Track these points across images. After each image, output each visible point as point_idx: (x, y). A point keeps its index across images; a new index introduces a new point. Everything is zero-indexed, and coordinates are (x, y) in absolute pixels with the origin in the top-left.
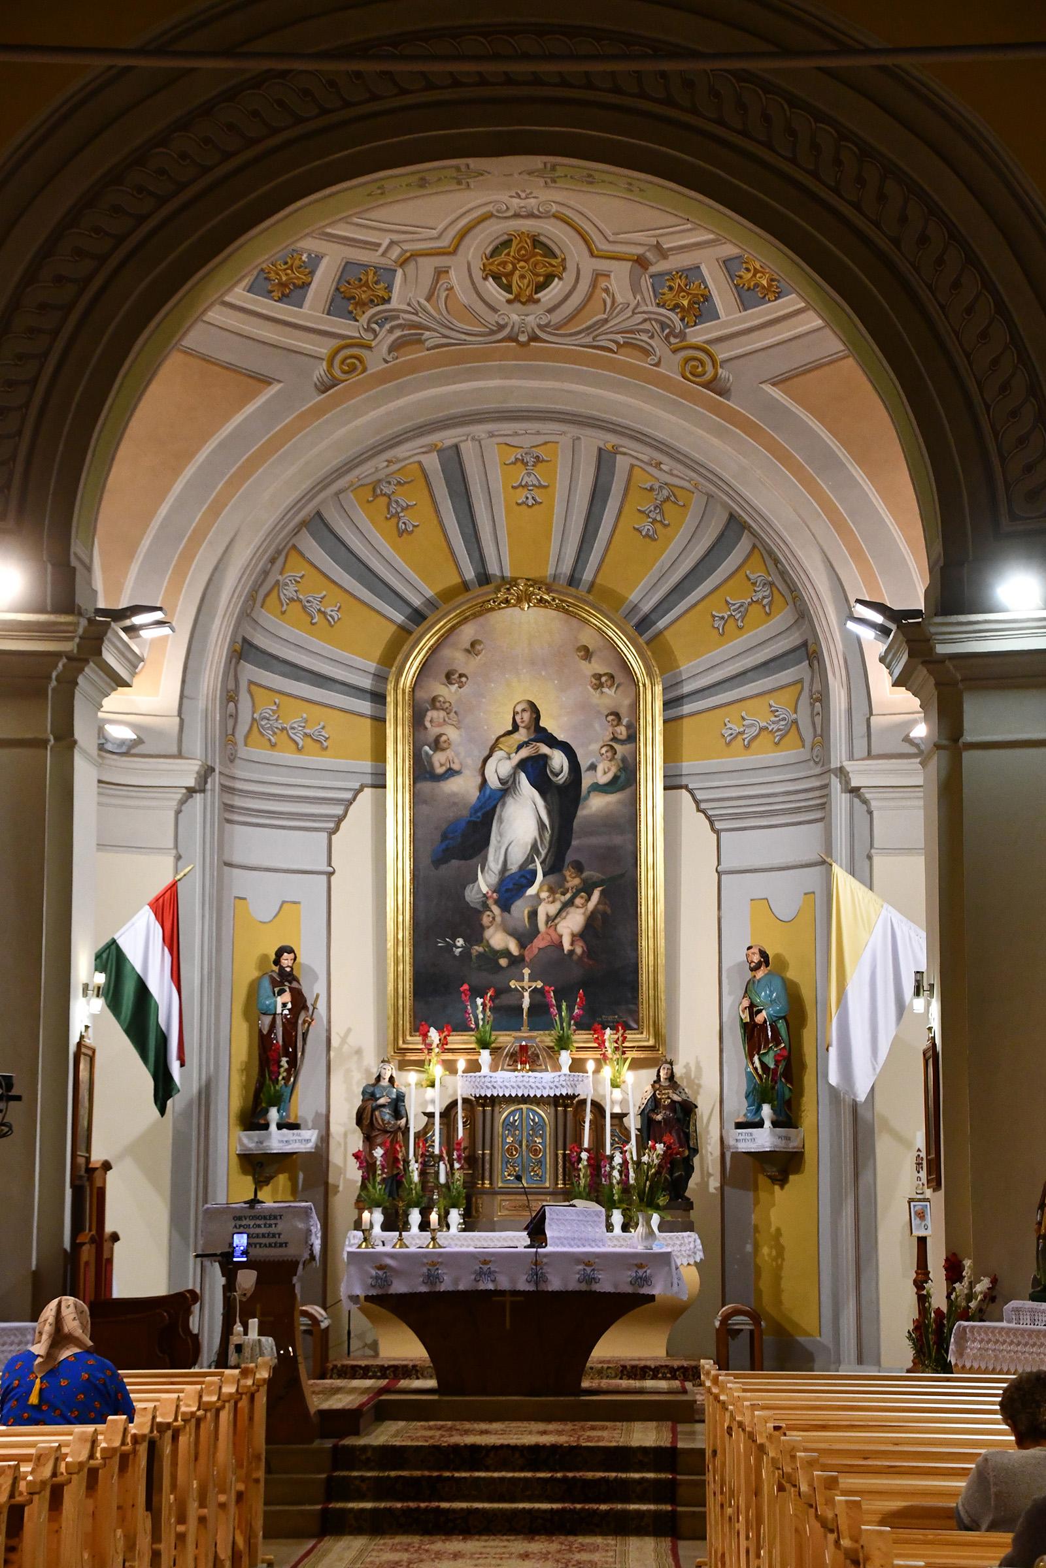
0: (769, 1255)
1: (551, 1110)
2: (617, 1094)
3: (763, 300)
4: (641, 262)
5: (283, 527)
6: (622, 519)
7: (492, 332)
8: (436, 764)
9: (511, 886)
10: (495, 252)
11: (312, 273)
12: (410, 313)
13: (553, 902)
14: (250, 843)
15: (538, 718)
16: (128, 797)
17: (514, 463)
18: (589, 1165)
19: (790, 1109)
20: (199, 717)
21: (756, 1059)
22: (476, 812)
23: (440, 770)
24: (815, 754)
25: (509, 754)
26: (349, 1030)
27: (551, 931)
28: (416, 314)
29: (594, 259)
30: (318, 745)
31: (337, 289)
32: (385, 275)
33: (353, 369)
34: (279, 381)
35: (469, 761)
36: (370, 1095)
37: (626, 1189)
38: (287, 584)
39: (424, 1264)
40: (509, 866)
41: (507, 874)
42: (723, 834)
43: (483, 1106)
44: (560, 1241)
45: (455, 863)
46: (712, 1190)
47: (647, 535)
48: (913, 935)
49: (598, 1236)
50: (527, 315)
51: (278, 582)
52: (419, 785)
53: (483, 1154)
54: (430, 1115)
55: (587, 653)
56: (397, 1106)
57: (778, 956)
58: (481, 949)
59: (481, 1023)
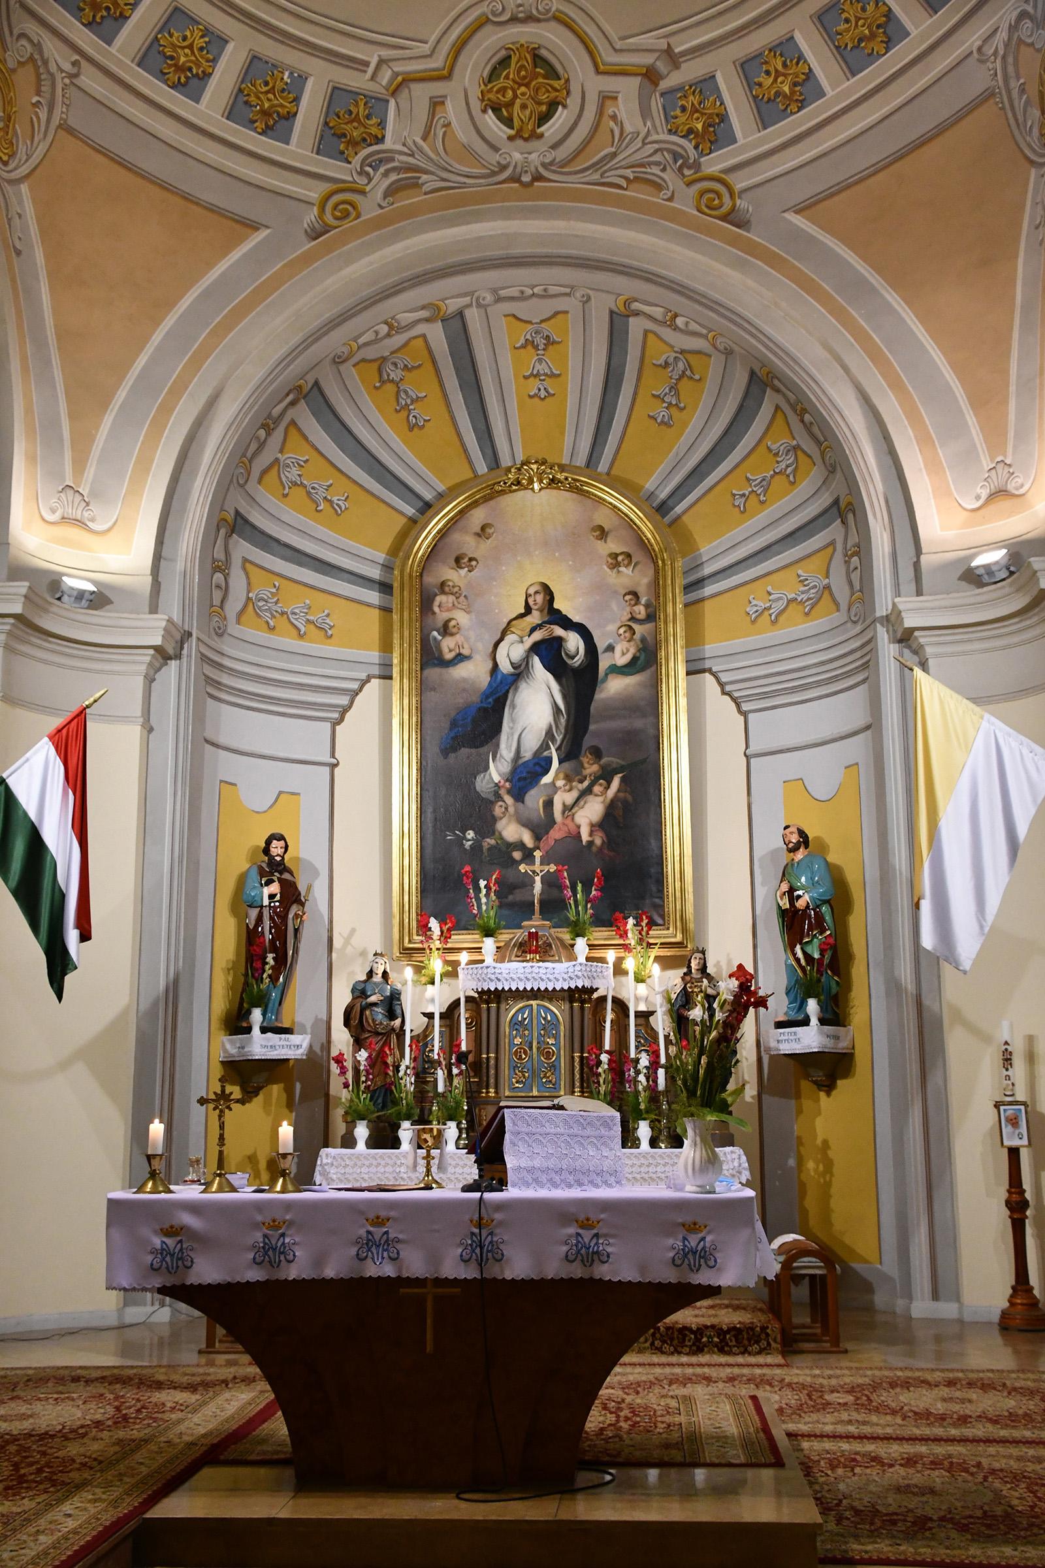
0: (816, 1170)
1: (565, 1006)
2: (642, 989)
3: (785, 113)
4: (651, 76)
5: (271, 382)
6: (631, 424)
7: (494, 174)
8: (445, 650)
9: (524, 775)
10: (494, 74)
11: (297, 100)
12: (406, 154)
13: (570, 790)
14: (236, 725)
15: (551, 600)
16: (82, 658)
17: (523, 347)
18: (611, 1069)
19: (837, 1005)
20: (178, 579)
21: (798, 949)
22: (487, 697)
23: (449, 656)
24: (853, 614)
25: (521, 638)
26: (353, 931)
27: (568, 821)
28: (412, 155)
29: (600, 77)
30: (323, 633)
31: (326, 123)
32: (376, 105)
33: (346, 215)
34: (267, 227)
35: (480, 646)
36: (360, 992)
37: (654, 1096)
38: (288, 466)
39: (256, 1226)
40: (523, 754)
41: (521, 761)
42: (751, 716)
43: (488, 1002)
44: (534, 1176)
45: (464, 751)
46: (748, 1099)
47: (662, 422)
48: (1025, 751)
49: (607, 1165)
50: (530, 153)
51: (277, 460)
52: (426, 672)
53: (488, 1058)
54: (430, 1016)
55: (602, 533)
56: (392, 1004)
57: (818, 839)
58: (493, 842)
59: (484, 907)
